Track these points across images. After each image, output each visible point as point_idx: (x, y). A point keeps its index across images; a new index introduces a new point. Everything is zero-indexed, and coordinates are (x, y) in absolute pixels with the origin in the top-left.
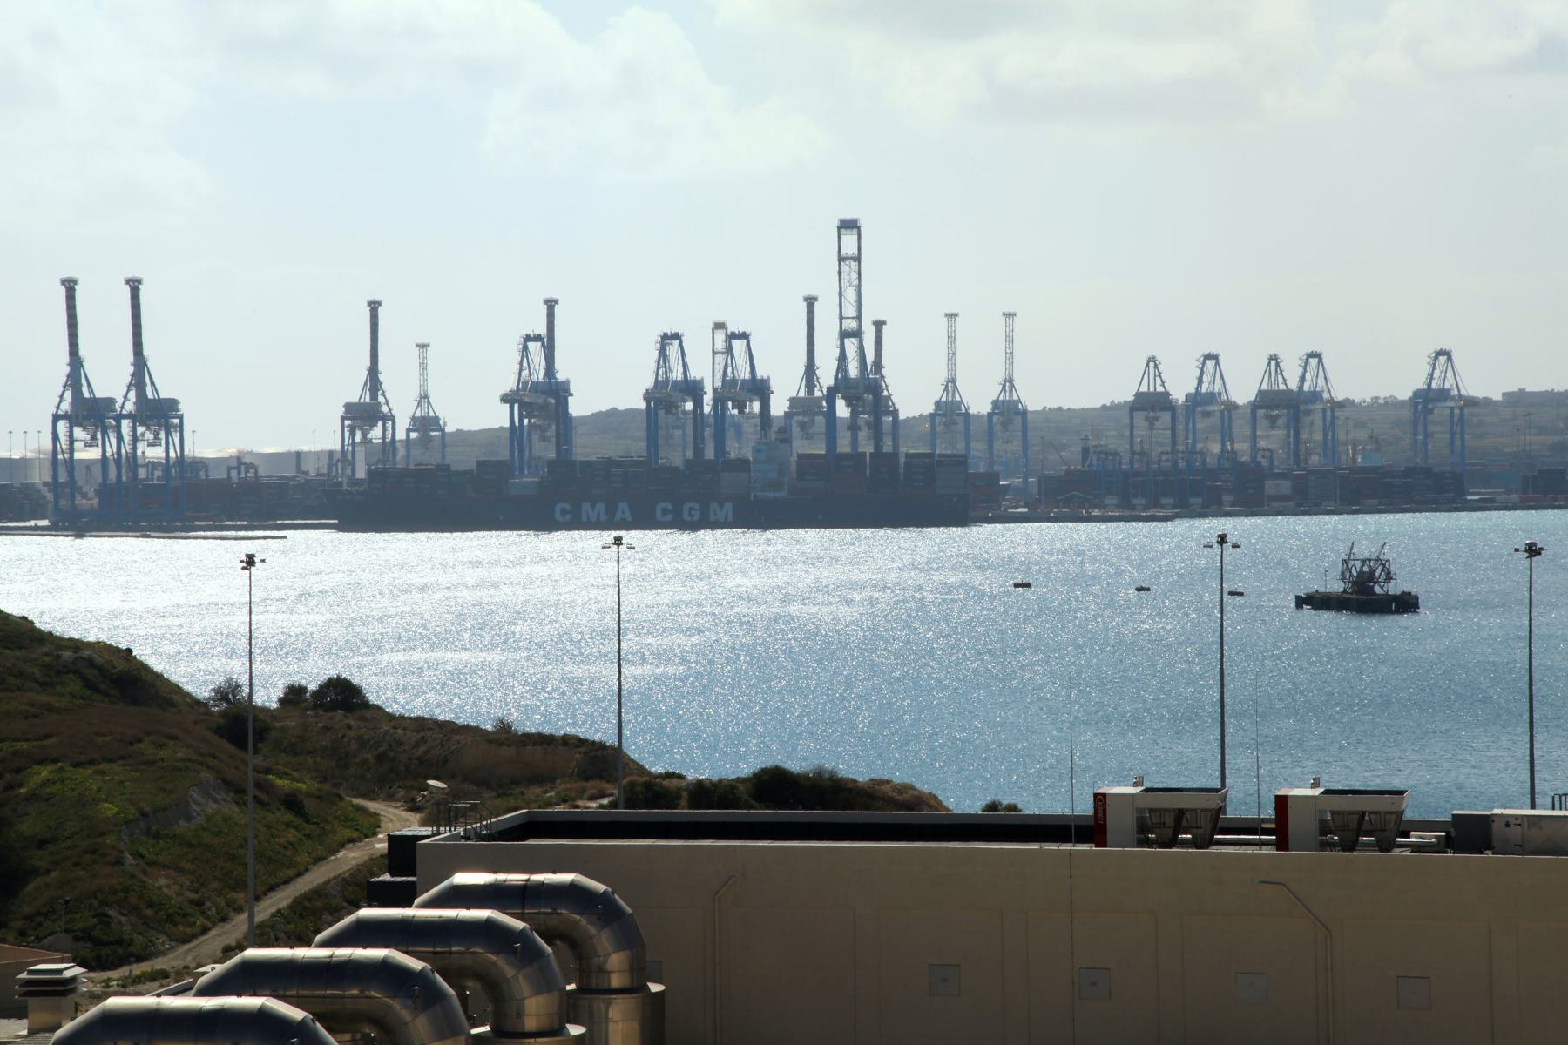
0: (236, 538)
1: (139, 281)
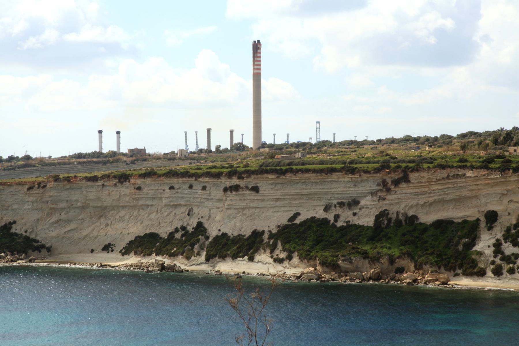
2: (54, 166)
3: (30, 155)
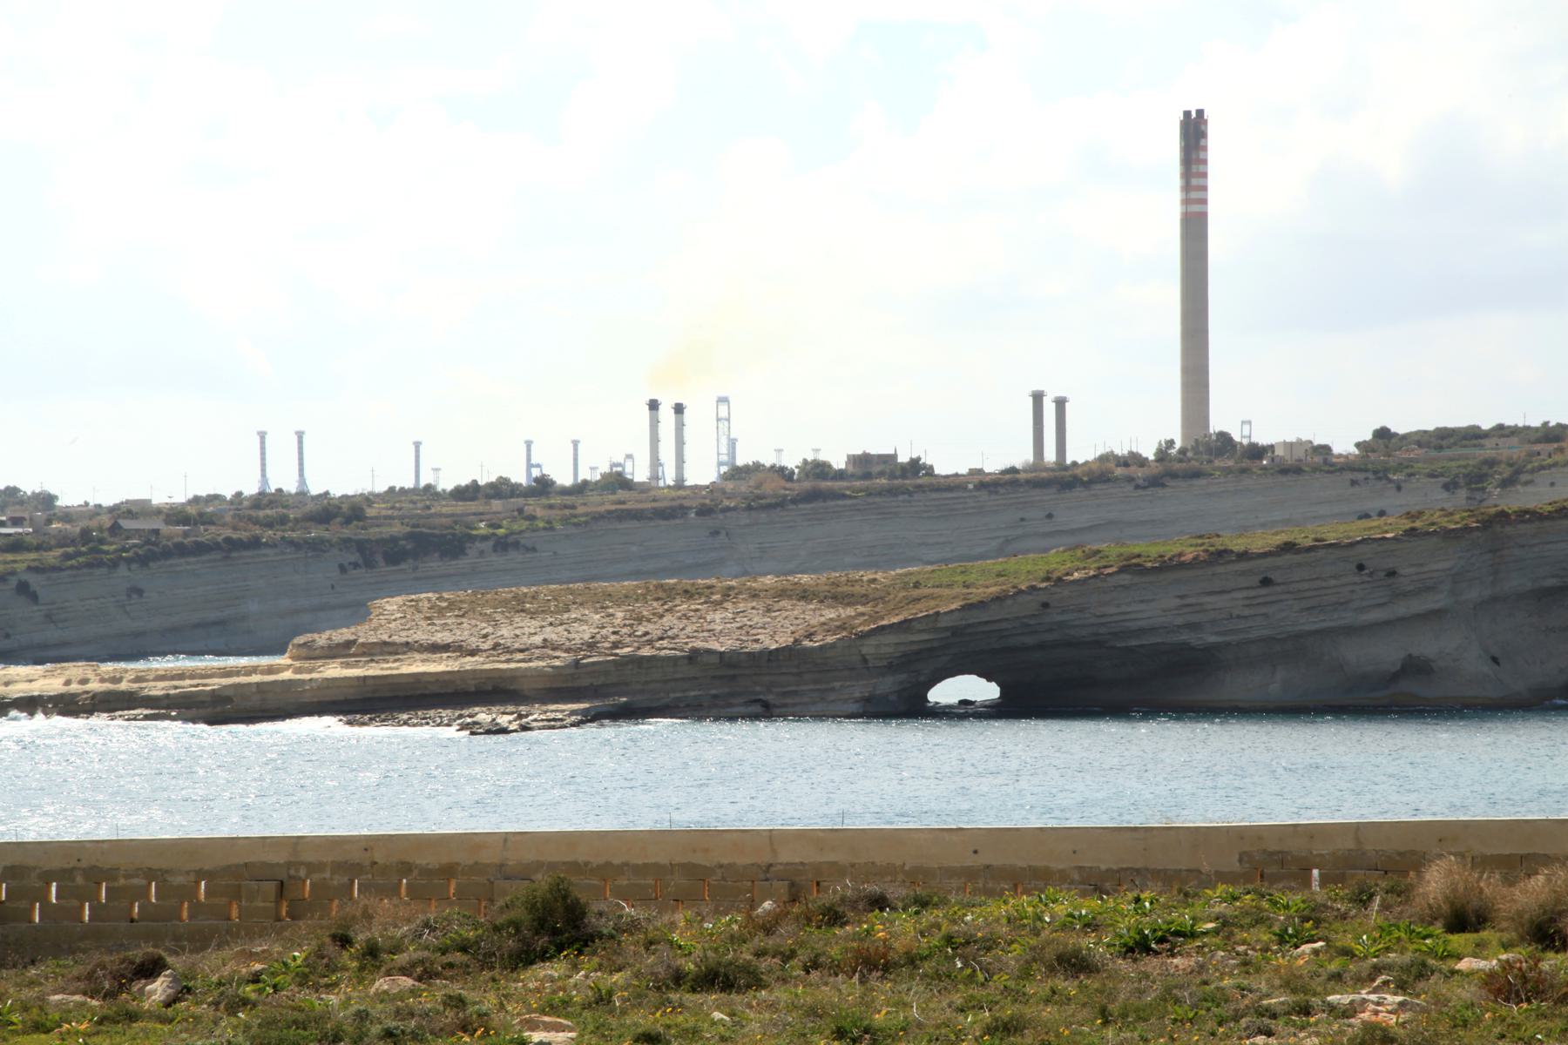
0: (67, 705)
1: (303, 433)
2: (906, 497)
3: (1401, 426)
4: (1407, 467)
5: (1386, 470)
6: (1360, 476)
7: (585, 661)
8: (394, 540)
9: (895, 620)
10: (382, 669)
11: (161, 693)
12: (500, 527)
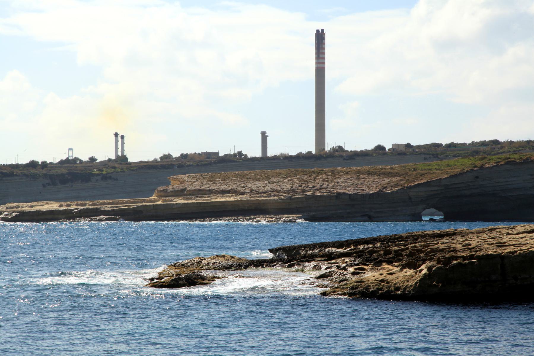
3: (367, 149)
4: (445, 153)
5: (437, 154)
6: (428, 156)
7: (293, 197)
8: (63, 175)
9: (423, 181)
10: (203, 200)
11: (111, 209)
12: (103, 171)
